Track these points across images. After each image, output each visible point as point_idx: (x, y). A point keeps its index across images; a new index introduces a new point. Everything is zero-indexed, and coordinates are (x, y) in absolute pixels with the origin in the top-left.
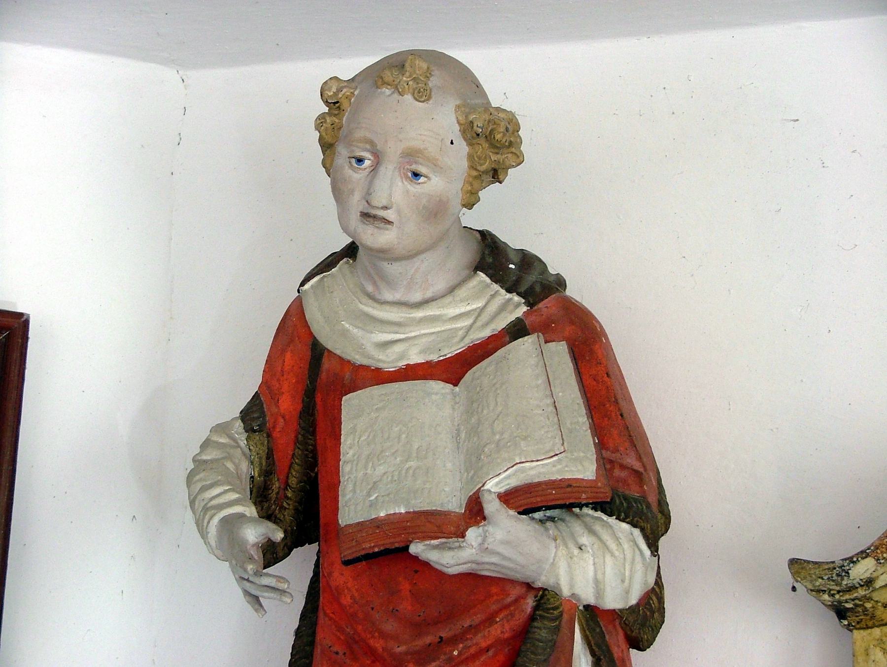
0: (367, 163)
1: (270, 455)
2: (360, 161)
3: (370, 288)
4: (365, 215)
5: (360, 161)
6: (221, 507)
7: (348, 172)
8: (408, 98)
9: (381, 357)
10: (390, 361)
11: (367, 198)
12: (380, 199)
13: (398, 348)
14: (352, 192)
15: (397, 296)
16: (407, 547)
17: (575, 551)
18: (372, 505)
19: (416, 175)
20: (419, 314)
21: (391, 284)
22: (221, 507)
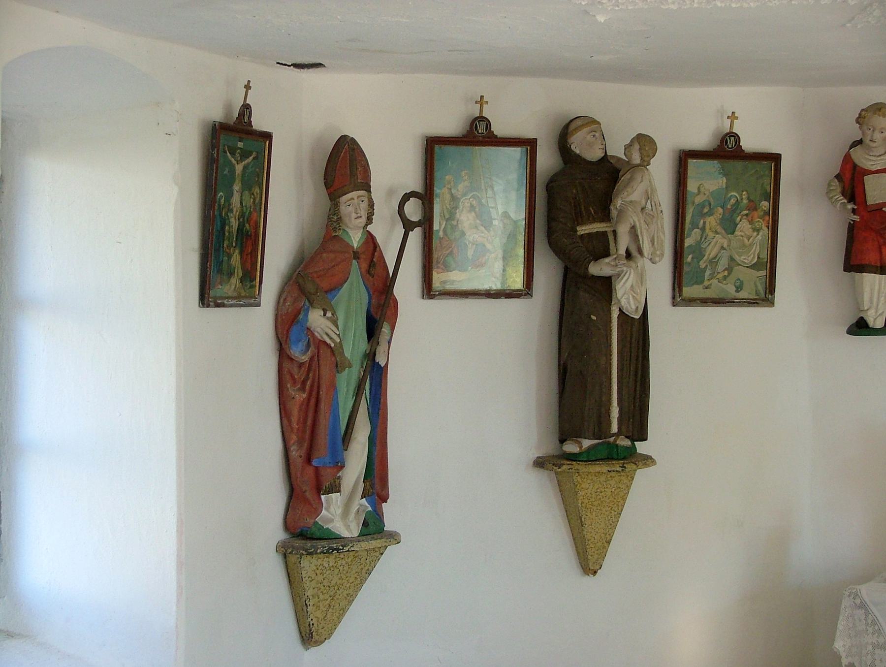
0: (871, 130)
1: (844, 187)
2: (870, 129)
3: (867, 152)
4: (871, 141)
5: (870, 129)
6: (840, 200)
7: (867, 131)
8: (881, 117)
9: (872, 168)
10: (873, 168)
11: (872, 136)
12: (875, 138)
13: (875, 166)
14: (868, 136)
15: (874, 154)
16: (882, 209)
17: (578, 123)
18: (875, 200)
19: (882, 132)
20: (879, 158)
21: (873, 152)
22: (840, 200)
